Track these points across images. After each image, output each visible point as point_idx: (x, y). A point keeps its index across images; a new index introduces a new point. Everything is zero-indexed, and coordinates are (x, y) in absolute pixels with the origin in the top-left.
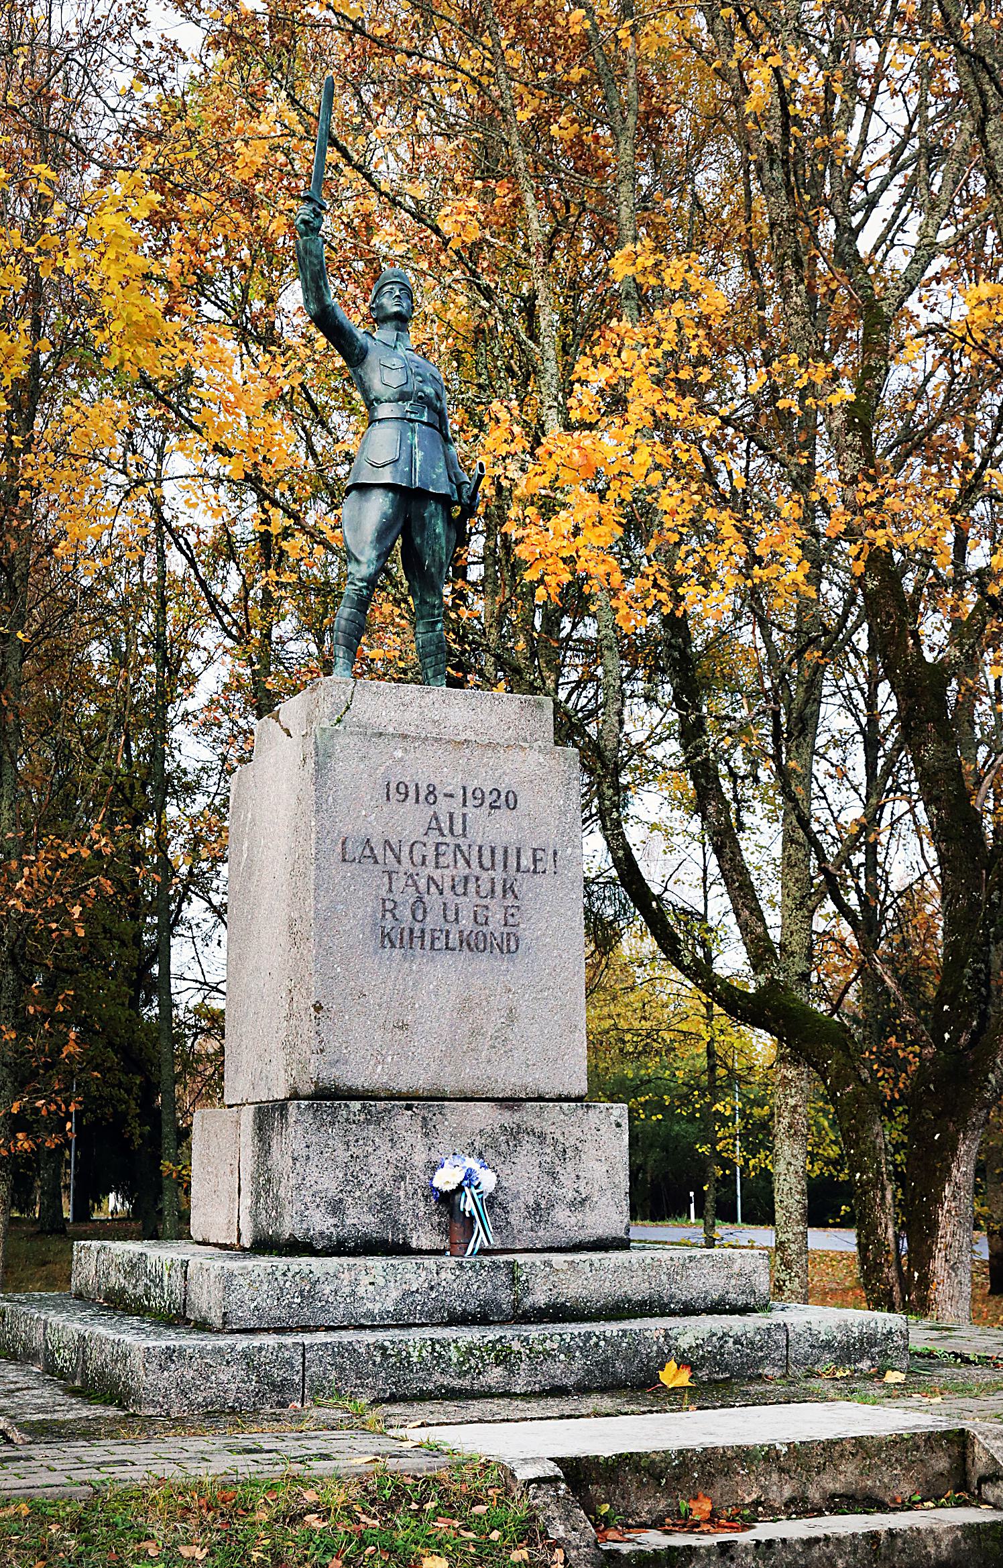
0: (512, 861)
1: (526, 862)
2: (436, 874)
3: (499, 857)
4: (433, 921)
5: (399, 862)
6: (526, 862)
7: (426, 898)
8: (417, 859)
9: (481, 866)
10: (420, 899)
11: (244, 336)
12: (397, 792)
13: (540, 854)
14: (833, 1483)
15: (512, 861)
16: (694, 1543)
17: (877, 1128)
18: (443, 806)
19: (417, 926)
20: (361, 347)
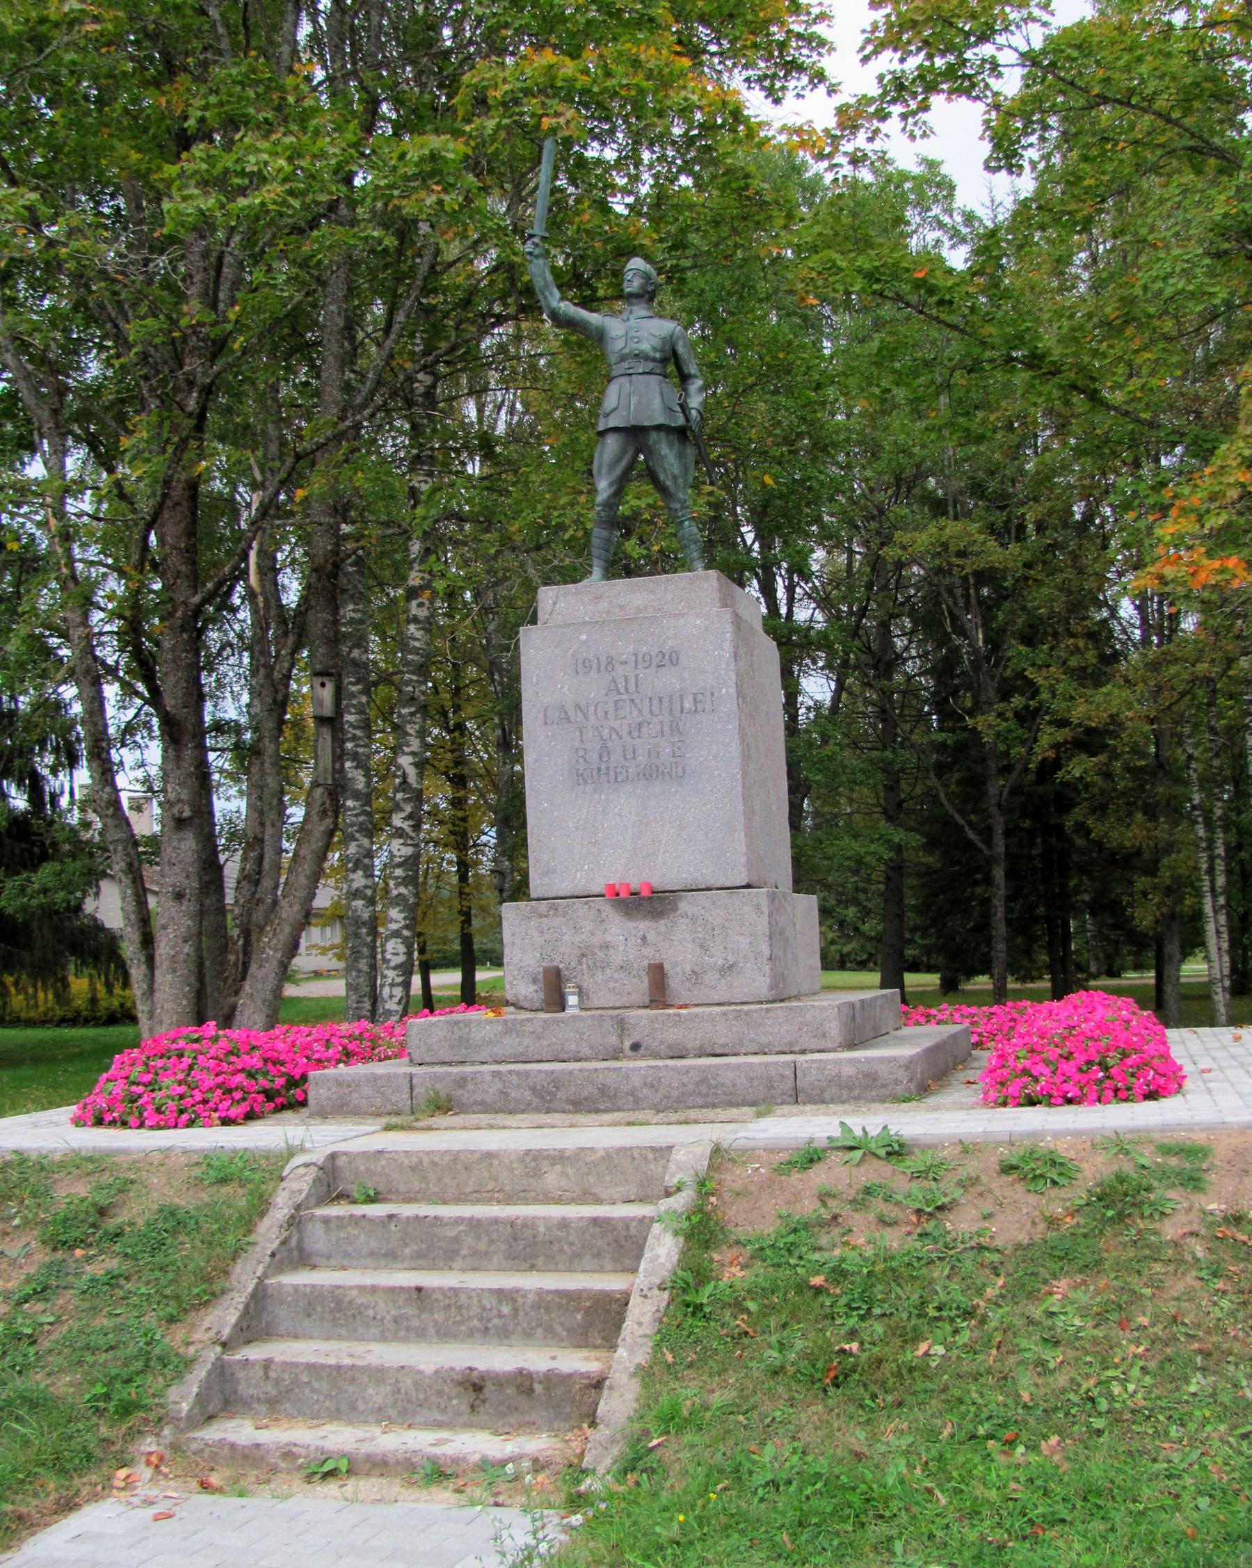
0: (677, 706)
1: (687, 705)
2: (616, 724)
3: (666, 704)
4: (616, 759)
5: (586, 717)
6: (687, 705)
7: (609, 744)
8: (601, 714)
9: (651, 712)
10: (604, 747)
11: (868, 1191)
12: (583, 666)
13: (700, 697)
14: (303, 881)
15: (677, 706)
16: (422, 1213)
17: (370, 1391)
18: (620, 671)
19: (603, 766)
20: (597, 328)
